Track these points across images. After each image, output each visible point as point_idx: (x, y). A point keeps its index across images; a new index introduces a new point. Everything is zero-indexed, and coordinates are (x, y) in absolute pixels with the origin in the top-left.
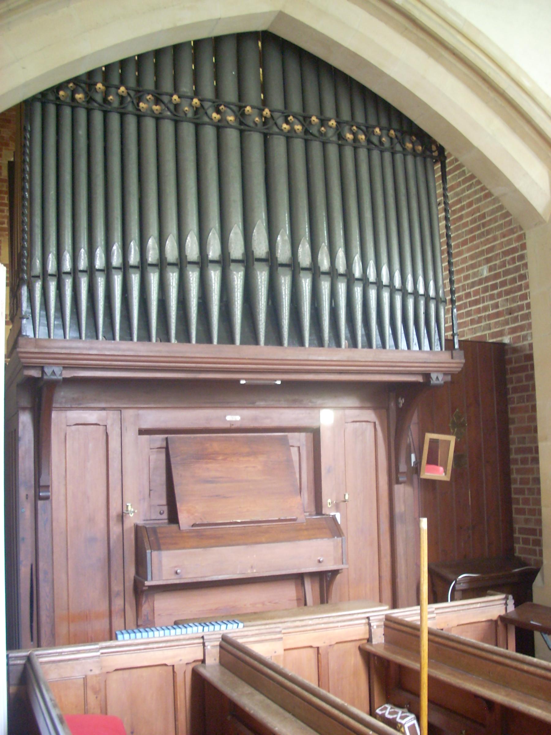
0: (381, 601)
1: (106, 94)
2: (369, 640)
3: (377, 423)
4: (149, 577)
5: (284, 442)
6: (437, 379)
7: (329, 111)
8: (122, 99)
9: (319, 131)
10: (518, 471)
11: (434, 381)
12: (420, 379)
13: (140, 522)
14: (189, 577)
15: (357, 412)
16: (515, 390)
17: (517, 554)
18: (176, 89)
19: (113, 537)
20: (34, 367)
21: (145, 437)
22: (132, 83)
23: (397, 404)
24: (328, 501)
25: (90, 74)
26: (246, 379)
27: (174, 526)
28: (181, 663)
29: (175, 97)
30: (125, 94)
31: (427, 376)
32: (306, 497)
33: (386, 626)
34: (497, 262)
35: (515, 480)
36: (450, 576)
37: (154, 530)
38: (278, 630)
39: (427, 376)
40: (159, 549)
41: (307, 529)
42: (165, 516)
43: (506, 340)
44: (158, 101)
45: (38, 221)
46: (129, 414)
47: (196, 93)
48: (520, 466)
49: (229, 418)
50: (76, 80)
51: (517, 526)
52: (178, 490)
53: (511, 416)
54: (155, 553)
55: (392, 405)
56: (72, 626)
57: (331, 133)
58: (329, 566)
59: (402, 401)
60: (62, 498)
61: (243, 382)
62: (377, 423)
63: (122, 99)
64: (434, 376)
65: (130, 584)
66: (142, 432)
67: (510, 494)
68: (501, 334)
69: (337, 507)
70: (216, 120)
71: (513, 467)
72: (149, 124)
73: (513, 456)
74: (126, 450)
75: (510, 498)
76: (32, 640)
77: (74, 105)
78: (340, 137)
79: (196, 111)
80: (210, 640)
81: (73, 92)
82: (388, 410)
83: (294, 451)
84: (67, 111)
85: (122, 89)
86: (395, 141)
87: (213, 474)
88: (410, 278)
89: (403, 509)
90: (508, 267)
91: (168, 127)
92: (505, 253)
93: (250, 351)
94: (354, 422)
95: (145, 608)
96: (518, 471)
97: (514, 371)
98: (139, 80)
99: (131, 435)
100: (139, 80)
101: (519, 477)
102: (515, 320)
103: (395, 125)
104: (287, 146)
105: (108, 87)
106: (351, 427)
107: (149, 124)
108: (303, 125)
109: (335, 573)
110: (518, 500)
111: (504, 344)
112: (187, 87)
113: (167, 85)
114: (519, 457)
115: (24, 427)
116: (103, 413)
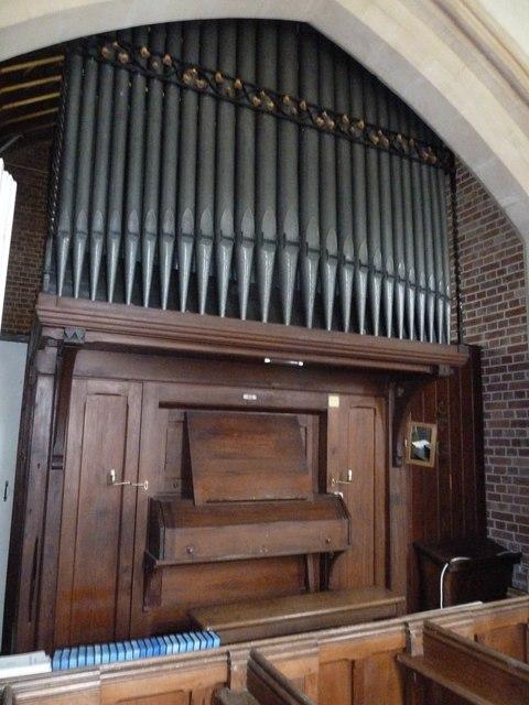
0: (388, 585)
1: (149, 61)
2: (407, 649)
3: (377, 409)
4: (161, 557)
5: (295, 424)
6: (444, 371)
7: (357, 114)
8: (165, 67)
9: (349, 130)
10: (492, 461)
11: (441, 372)
12: (427, 370)
13: (152, 495)
14: (201, 556)
15: (359, 398)
16: (491, 388)
17: (490, 536)
18: (219, 69)
19: (125, 510)
20: (54, 327)
21: (166, 411)
22: (176, 52)
23: (396, 394)
24: (333, 481)
25: (135, 31)
26: (271, 359)
27: (190, 502)
28: (200, 687)
29: (219, 75)
30: (169, 64)
31: (435, 367)
32: (309, 478)
33: (425, 634)
34: (475, 277)
35: (489, 469)
36: (442, 559)
37: (169, 505)
38: (313, 642)
39: (435, 367)
40: (173, 526)
41: (316, 509)
42: (179, 489)
43: (481, 343)
44: (201, 76)
45: (69, 176)
46: (150, 386)
47: (238, 75)
48: (494, 456)
49: (246, 397)
50: (119, 34)
51: (490, 510)
52: (194, 464)
53: (485, 410)
54: (168, 531)
55: (391, 395)
56: (75, 605)
57: (358, 134)
58: (336, 546)
59: (401, 391)
60: (76, 469)
61: (267, 361)
62: (377, 409)
63: (165, 67)
64: (442, 367)
65: (139, 560)
66: (162, 405)
67: (483, 480)
68: (478, 338)
69: (340, 487)
70: (256, 104)
71: (488, 457)
72: (191, 97)
73: (487, 446)
74: (145, 423)
75: (484, 484)
76: (30, 620)
77: (117, 66)
78: (367, 137)
79: (236, 91)
80: (237, 659)
81: (117, 52)
82: (387, 398)
83: (302, 430)
84: (109, 70)
85: (168, 57)
86: (413, 149)
87: (228, 450)
88: (422, 275)
89: (398, 491)
90: (487, 281)
91: (208, 103)
92: (484, 269)
93: (276, 330)
94: (358, 407)
95: (154, 583)
96: (492, 461)
97: (490, 371)
98: (183, 52)
99: (151, 407)
100: (183, 52)
101: (493, 466)
102: (494, 326)
103: (413, 134)
104: (255, 215)
105: (153, 53)
106: (354, 412)
107: (191, 97)
108: (335, 121)
109: (338, 553)
110: (492, 487)
111: (481, 347)
112: (229, 69)
113: (210, 63)
114: (494, 448)
115: (42, 394)
116: (126, 384)
